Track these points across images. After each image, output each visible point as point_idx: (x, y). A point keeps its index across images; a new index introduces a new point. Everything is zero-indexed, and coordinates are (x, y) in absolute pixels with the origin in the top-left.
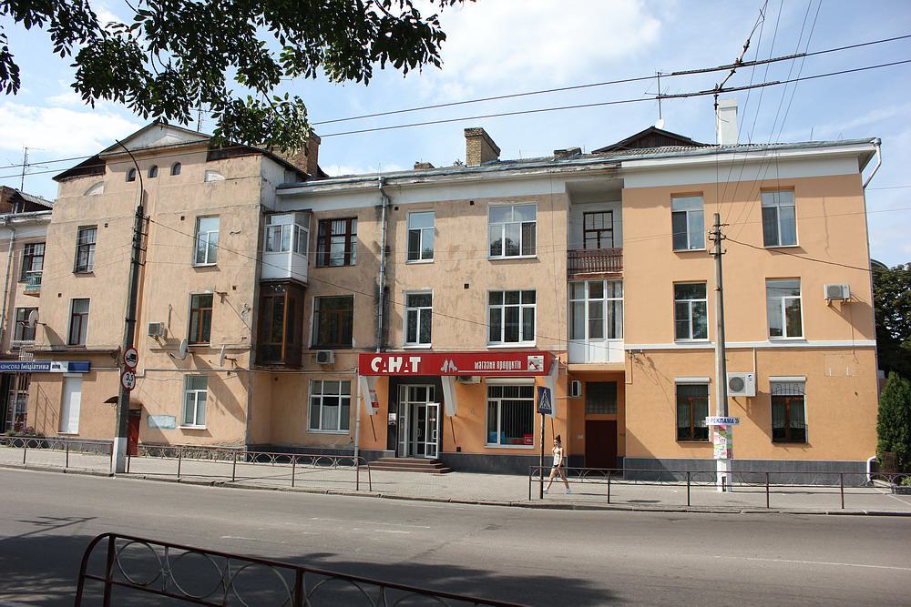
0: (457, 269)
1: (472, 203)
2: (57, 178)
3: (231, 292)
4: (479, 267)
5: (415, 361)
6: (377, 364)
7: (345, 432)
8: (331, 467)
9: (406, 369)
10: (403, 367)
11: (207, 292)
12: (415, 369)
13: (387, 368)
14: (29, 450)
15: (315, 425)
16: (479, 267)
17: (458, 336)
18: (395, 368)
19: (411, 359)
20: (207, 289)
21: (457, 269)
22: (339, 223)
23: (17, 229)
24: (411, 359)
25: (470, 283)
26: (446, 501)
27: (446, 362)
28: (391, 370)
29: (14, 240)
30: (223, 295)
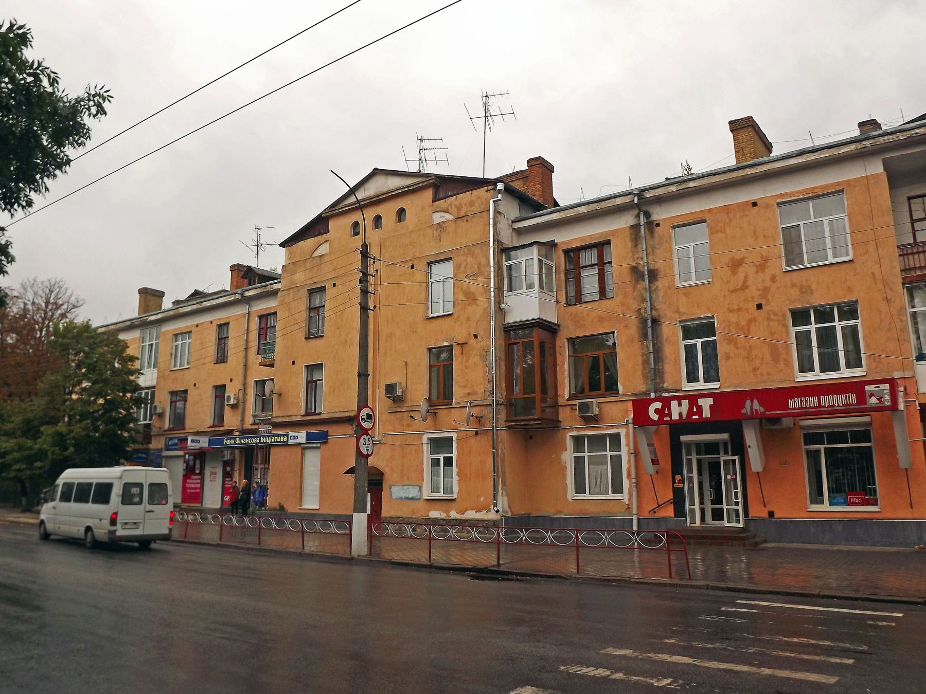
0: (744, 287)
2: (282, 245)
3: (473, 341)
5: (706, 404)
6: (657, 411)
7: (618, 496)
9: (695, 414)
10: (690, 412)
11: (446, 344)
12: (706, 413)
13: (670, 415)
18: (680, 414)
19: (701, 402)
22: (588, 252)
24: (701, 402)
25: (763, 302)
28: (675, 417)
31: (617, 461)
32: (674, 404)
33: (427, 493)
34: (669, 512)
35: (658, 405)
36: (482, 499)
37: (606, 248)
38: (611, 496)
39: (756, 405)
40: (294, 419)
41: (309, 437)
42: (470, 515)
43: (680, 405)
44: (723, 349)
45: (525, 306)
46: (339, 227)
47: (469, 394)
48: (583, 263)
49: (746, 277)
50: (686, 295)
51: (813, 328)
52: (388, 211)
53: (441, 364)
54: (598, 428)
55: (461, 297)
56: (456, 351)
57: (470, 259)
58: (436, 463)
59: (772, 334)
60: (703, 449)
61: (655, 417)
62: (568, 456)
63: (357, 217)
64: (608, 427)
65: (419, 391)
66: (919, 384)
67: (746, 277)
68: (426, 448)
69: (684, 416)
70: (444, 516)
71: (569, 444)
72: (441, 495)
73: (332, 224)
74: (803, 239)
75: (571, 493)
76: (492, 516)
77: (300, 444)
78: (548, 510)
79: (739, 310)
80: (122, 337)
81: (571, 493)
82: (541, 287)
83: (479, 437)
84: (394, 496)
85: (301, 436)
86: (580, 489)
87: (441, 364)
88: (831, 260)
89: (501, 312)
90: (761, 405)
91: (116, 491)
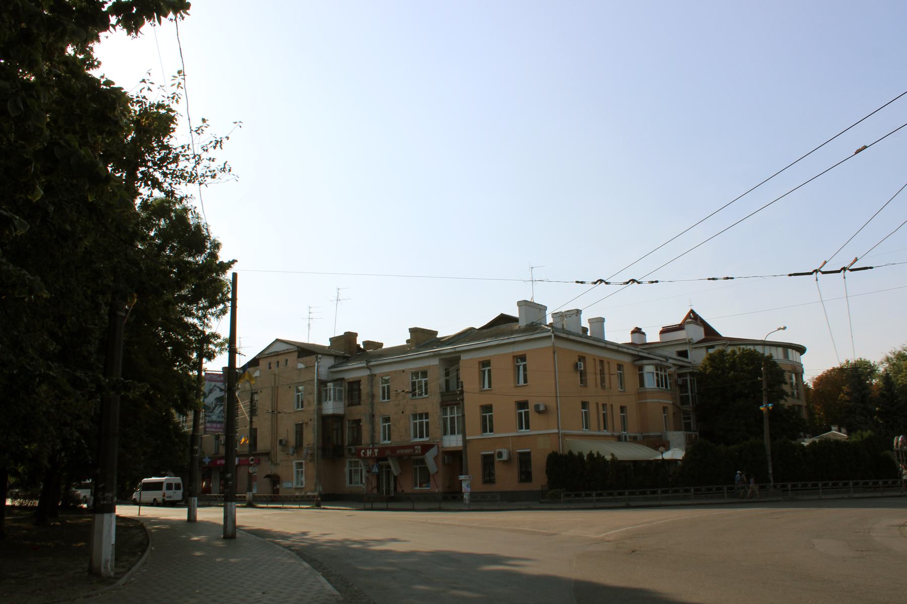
33: (294, 485)
34: (375, 491)
44: (392, 428)
45: (330, 407)
46: (263, 364)
51: (418, 421)
52: (281, 359)
56: (304, 426)
58: (298, 472)
62: (347, 470)
63: (269, 360)
65: (292, 441)
66: (461, 371)
68: (294, 468)
71: (347, 464)
73: (261, 362)
75: (348, 484)
76: (316, 494)
78: (222, 523)
80: (191, 415)
81: (348, 484)
82: (335, 399)
86: (351, 482)
89: (320, 410)
91: (164, 486)
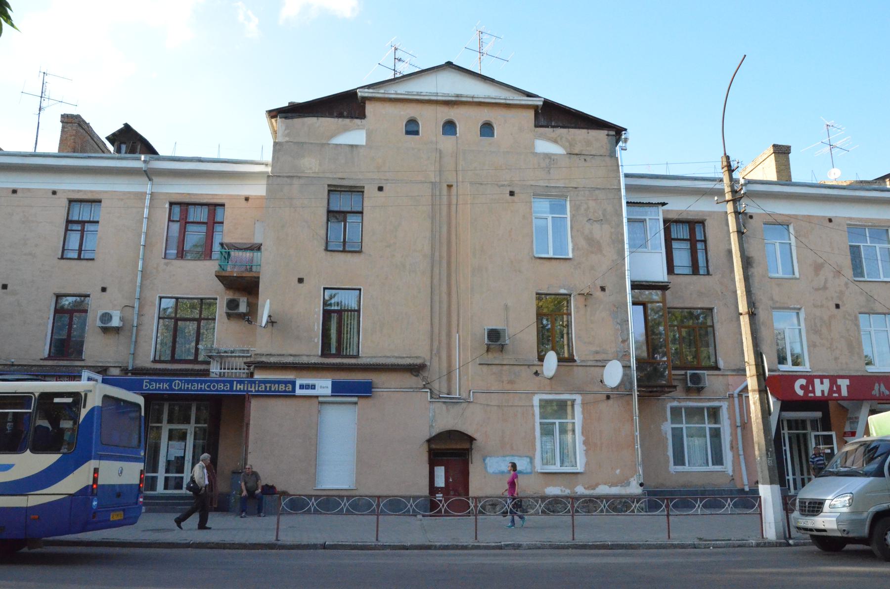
0: (825, 288)
1: (830, 220)
2: (274, 114)
3: (599, 294)
4: (847, 288)
5: (844, 383)
6: (802, 387)
7: (718, 468)
8: (751, 511)
9: (835, 392)
10: (831, 390)
11: (563, 291)
12: (844, 392)
13: (813, 391)
14: (480, 517)
15: (679, 459)
16: (847, 288)
17: (836, 359)
18: (823, 392)
19: (840, 382)
20: (564, 287)
21: (825, 288)
22: (199, 208)
23: (155, 179)
24: (840, 382)
25: (840, 303)
26: (494, 548)
27: (877, 385)
28: (818, 393)
29: (152, 194)
30: (587, 296)
31: (716, 434)
32: (817, 382)
35: (803, 382)
36: (618, 471)
37: (219, 210)
38: (711, 468)
39: (883, 388)
40: (305, 360)
41: (338, 389)
42: (603, 490)
43: (822, 383)
47: (597, 353)
48: (191, 219)
49: (826, 280)
50: (779, 285)
53: (552, 315)
54: (700, 400)
55: (582, 243)
57: (592, 204)
59: (848, 330)
60: (793, 424)
61: (800, 393)
64: (710, 400)
67: (826, 280)
69: (826, 394)
70: (567, 492)
72: (556, 468)
74: (879, 258)
77: (317, 397)
79: (822, 306)
83: (611, 402)
84: (490, 470)
85: (323, 385)
87: (552, 315)
88: (882, 279)
90: (887, 388)
